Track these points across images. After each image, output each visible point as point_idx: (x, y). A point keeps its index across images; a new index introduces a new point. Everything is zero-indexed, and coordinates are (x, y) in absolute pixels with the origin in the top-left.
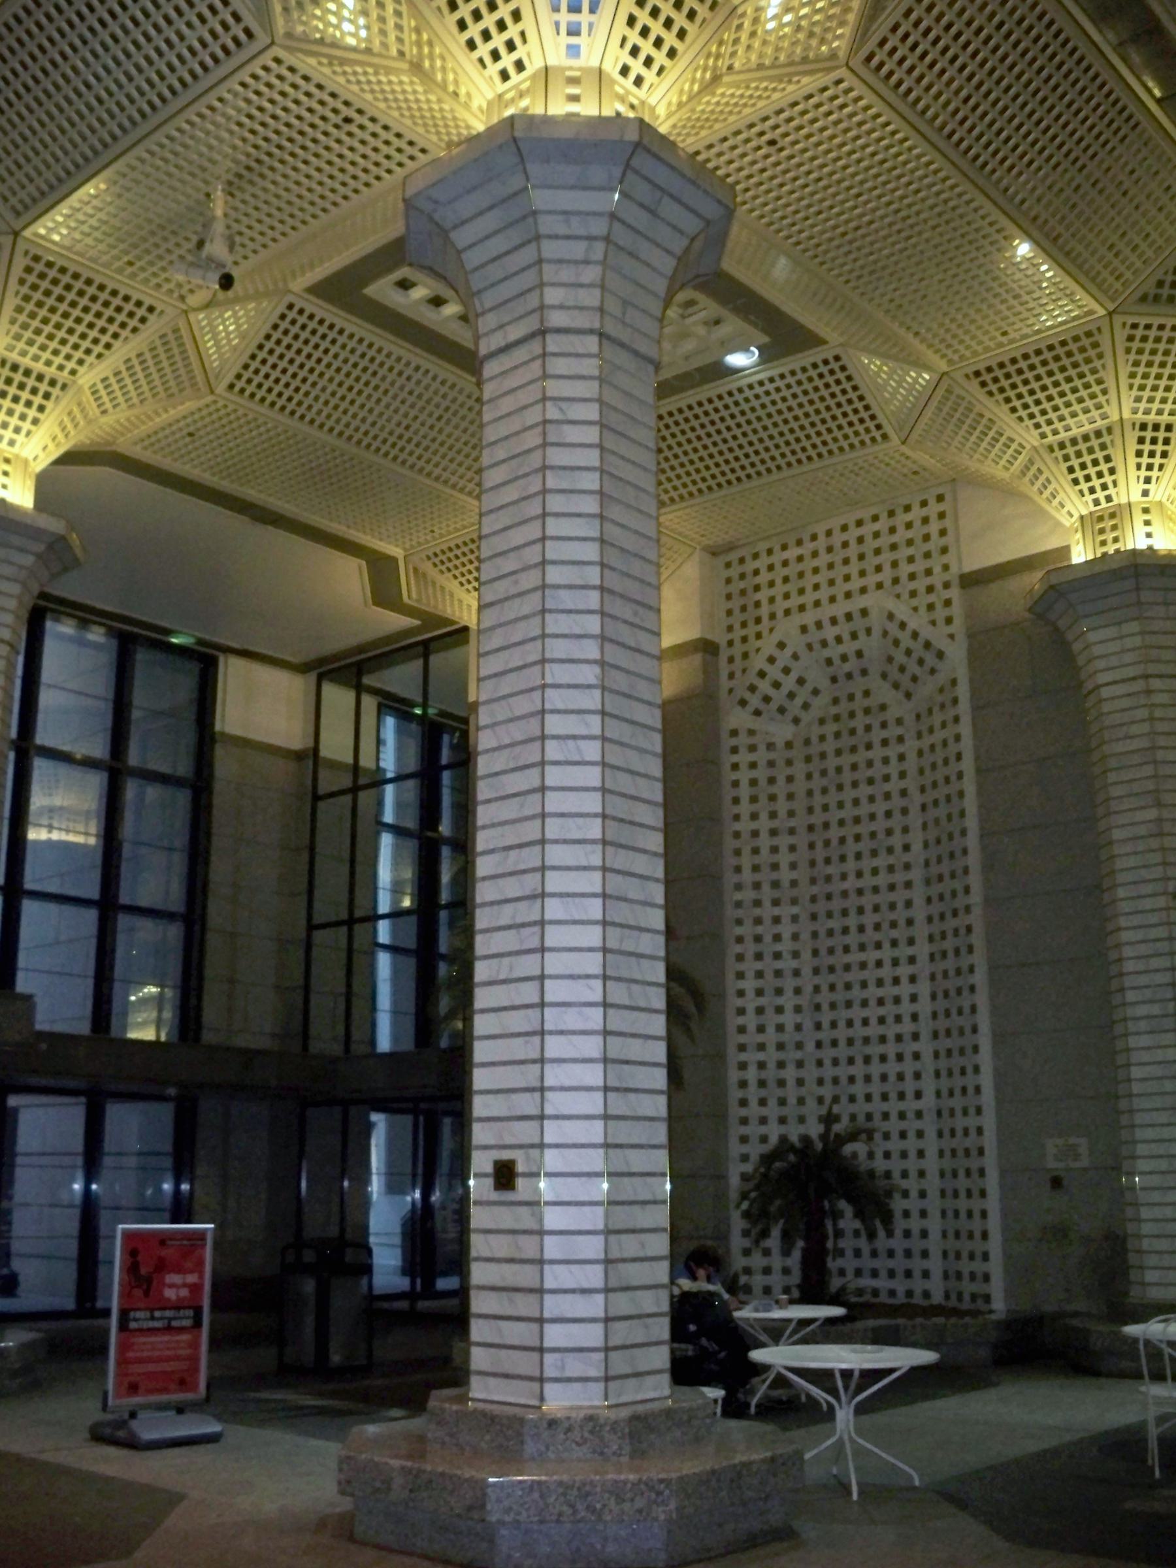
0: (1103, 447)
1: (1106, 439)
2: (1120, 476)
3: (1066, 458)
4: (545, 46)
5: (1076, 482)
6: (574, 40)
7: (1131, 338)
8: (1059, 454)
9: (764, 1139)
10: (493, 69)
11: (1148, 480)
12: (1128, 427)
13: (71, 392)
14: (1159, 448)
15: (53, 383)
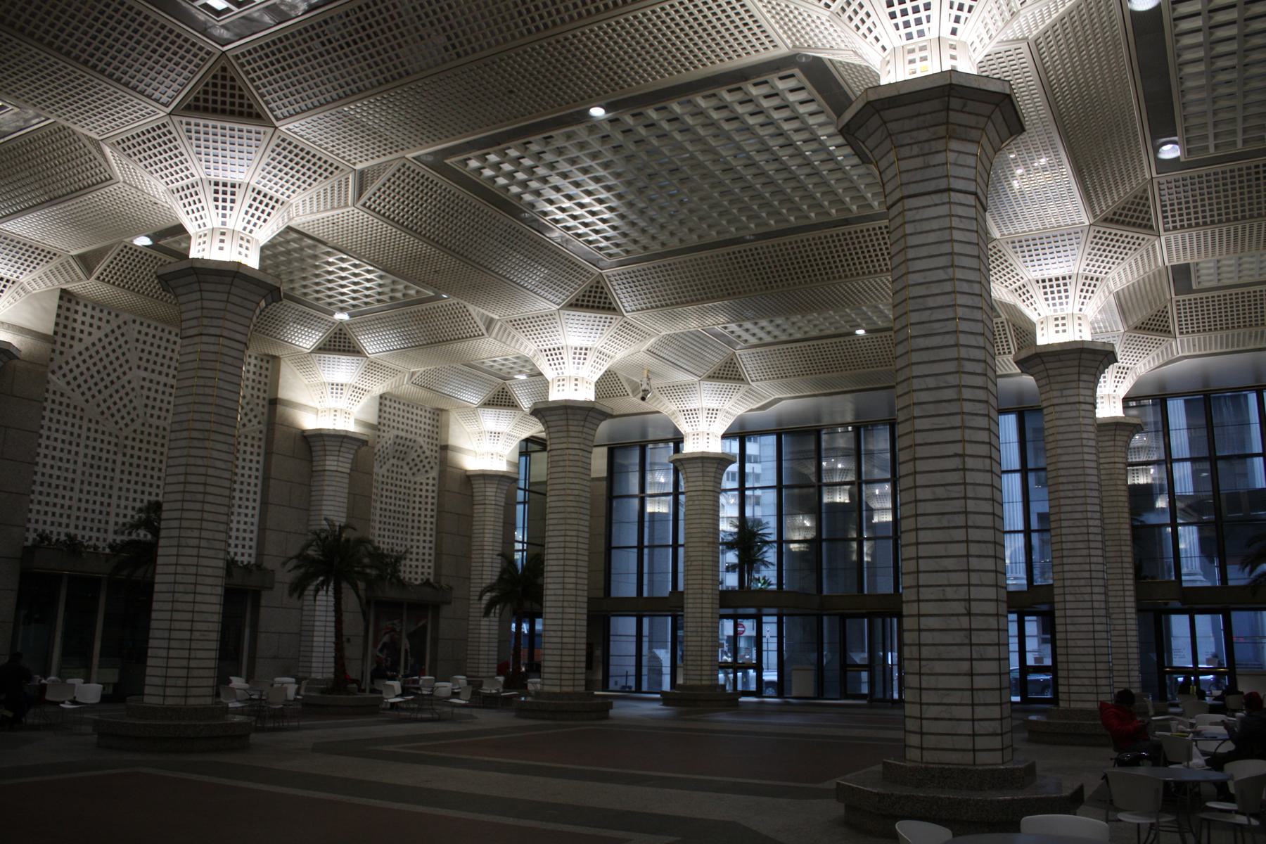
0: (1065, 285)
1: (1068, 281)
2: (1070, 300)
3: (1045, 287)
4: (939, 23)
5: (1047, 299)
6: (956, 25)
7: (278, 146)
8: (1041, 284)
9: (142, 501)
10: (245, 224)
11: (224, 216)
12: (250, 189)
13: (286, 206)
14: (1091, 289)
15: (277, 201)
